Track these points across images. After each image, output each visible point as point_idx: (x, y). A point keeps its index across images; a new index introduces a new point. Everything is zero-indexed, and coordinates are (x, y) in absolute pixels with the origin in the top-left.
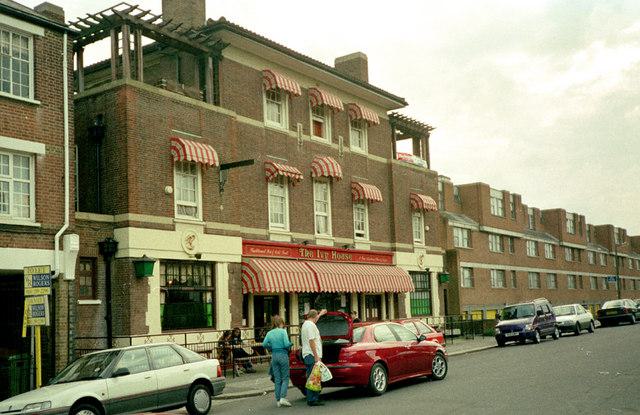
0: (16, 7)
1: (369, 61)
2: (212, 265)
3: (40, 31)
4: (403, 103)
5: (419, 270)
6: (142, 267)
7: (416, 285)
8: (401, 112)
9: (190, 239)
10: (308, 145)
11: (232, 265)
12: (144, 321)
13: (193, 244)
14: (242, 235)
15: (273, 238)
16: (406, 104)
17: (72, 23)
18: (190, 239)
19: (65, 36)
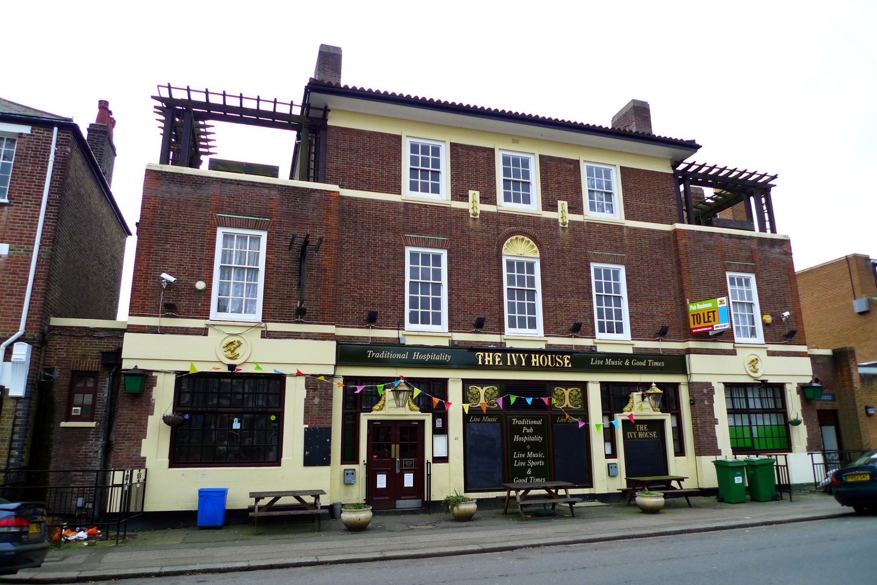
0: (38, 114)
1: (343, 54)
2: (781, 387)
3: (26, 129)
4: (692, 147)
5: (751, 381)
6: (146, 378)
7: (372, 398)
8: (697, 158)
9: (754, 362)
10: (762, 241)
11: (803, 389)
12: (139, 451)
13: (757, 367)
14: (811, 356)
15: (509, 345)
16: (699, 147)
17: (708, 198)
18: (754, 362)
19: (56, 129)
